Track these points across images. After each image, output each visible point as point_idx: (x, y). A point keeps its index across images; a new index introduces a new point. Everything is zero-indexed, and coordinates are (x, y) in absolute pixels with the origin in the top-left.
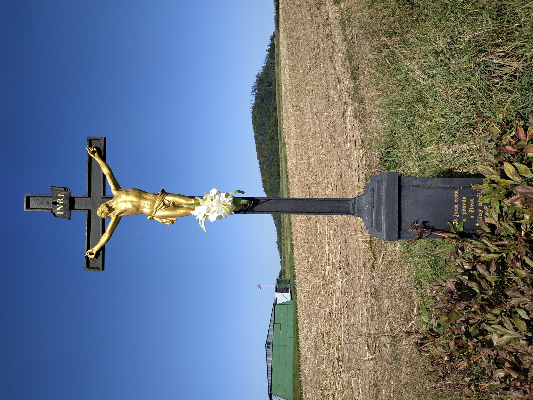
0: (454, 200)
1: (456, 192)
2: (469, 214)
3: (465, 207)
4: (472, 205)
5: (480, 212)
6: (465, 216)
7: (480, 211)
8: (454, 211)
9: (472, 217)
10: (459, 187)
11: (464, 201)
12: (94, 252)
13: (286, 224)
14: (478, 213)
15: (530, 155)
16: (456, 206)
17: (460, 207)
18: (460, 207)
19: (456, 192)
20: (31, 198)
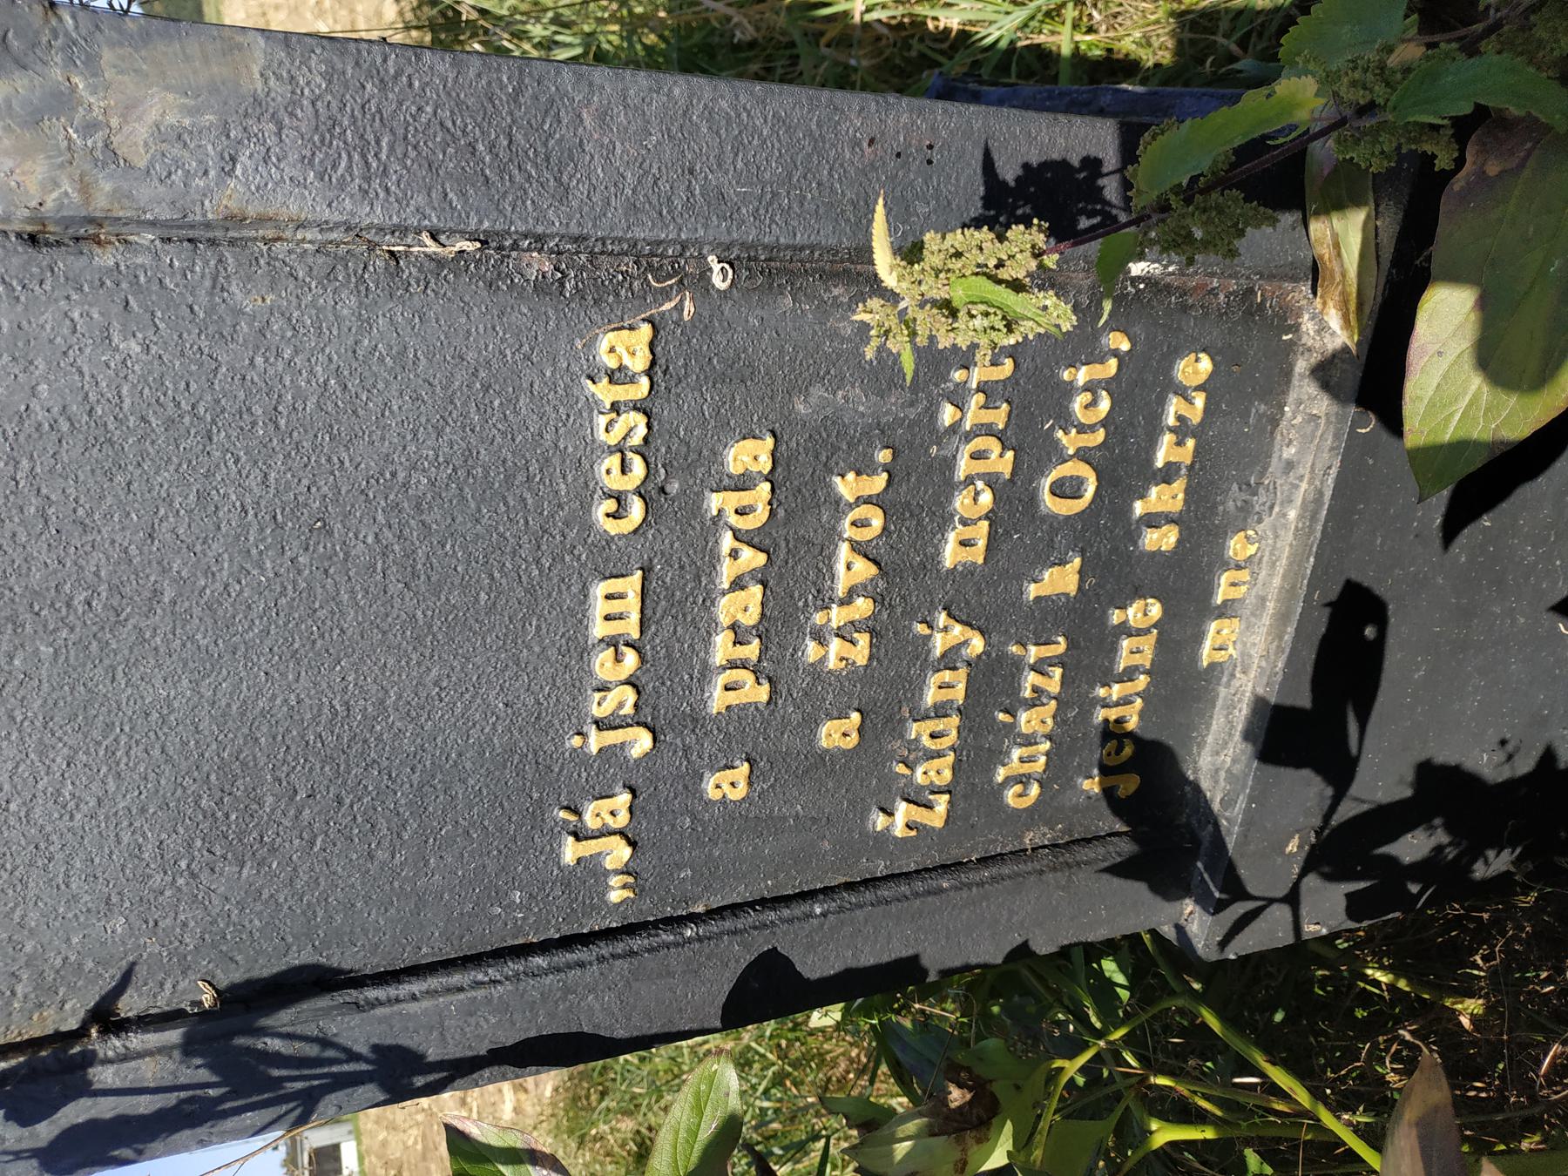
0: (587, 491)
1: (627, 347)
2: (797, 693)
3: (745, 606)
4: (850, 569)
5: (949, 660)
6: (740, 736)
7: (947, 634)
8: (580, 682)
9: (837, 734)
10: (668, 266)
11: (741, 509)
12: (1027, 329)
13: (1291, 934)
14: (919, 659)
15: (390, 12)
16: (614, 605)
17: (676, 605)
18: (676, 605)
19: (627, 347)
20: (718, 1024)
